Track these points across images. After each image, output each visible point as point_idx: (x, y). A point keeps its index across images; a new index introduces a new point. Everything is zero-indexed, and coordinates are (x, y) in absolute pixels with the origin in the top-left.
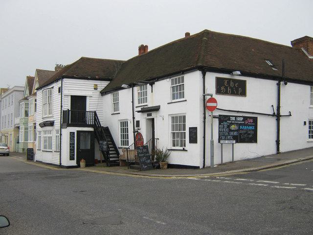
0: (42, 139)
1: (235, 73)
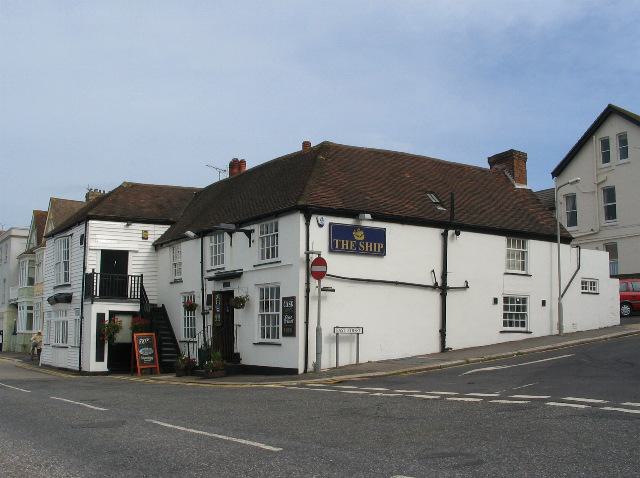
0: (53, 325)
1: (361, 216)
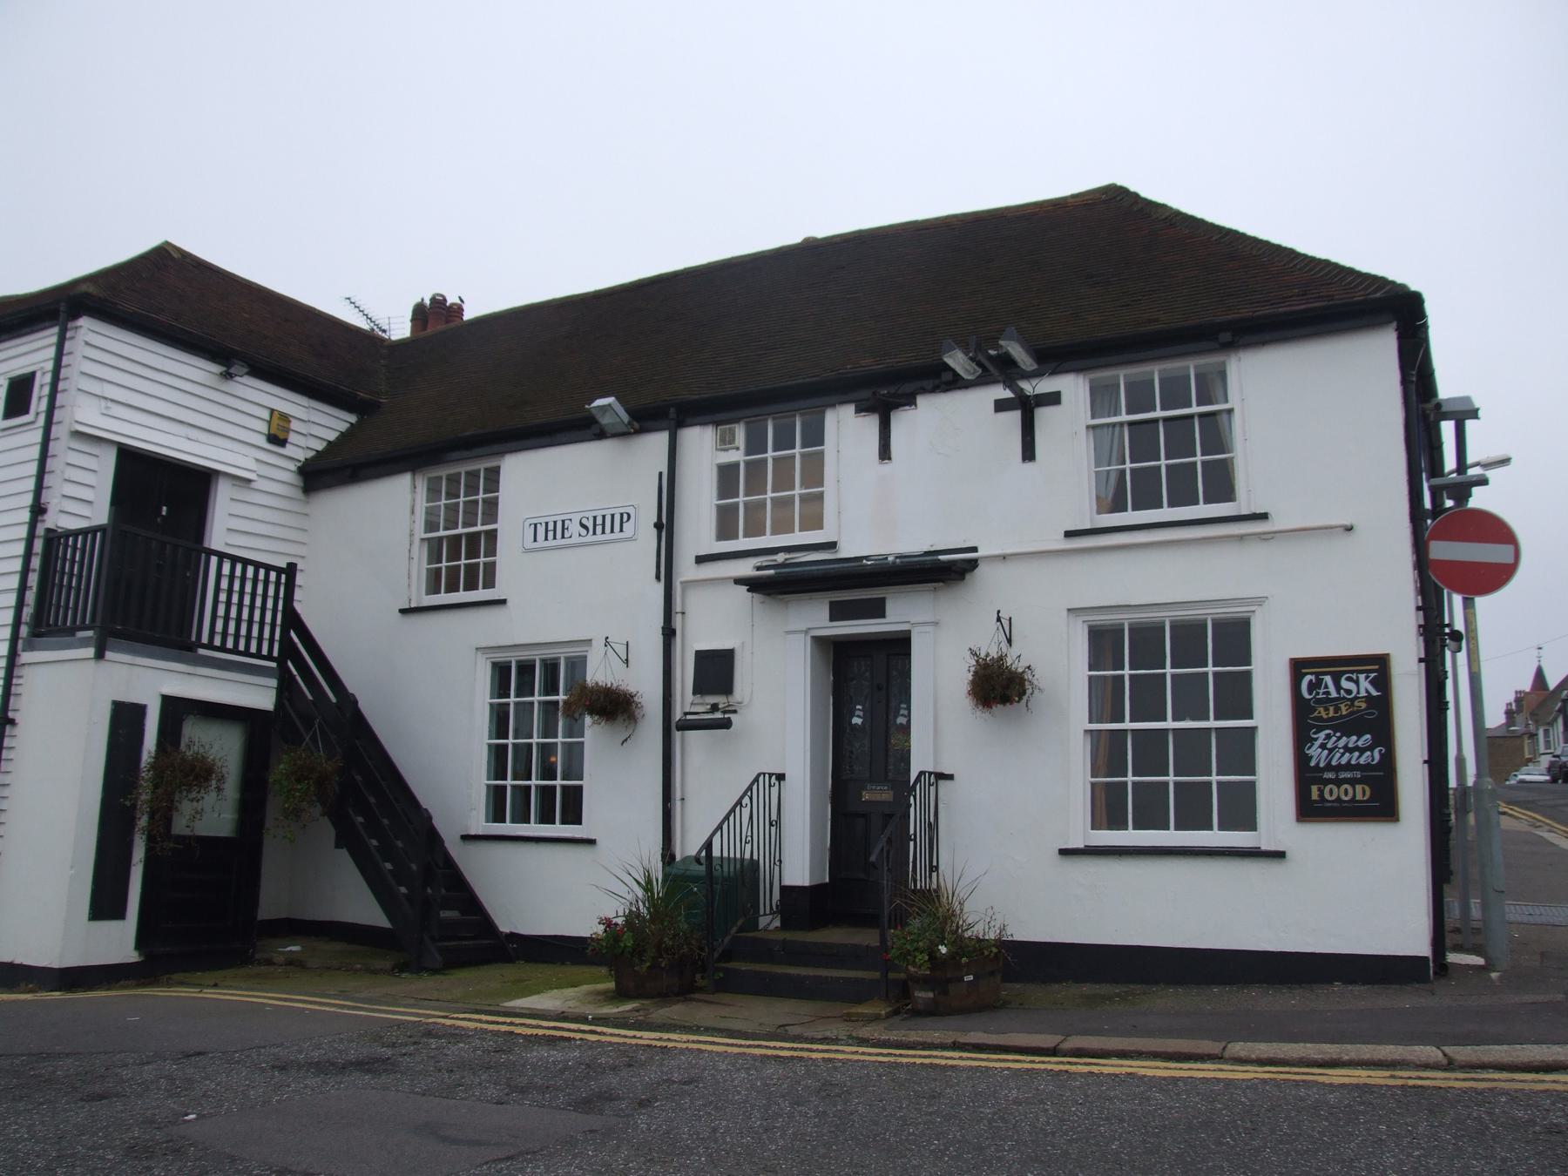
0: (1552, 746)
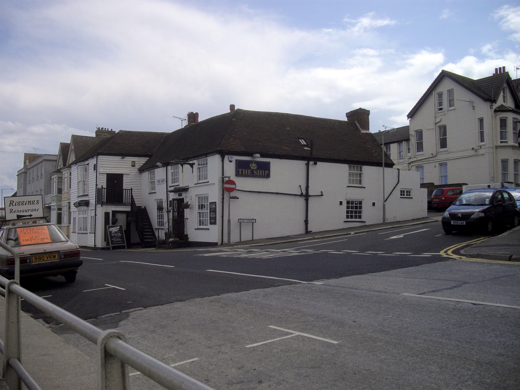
1: (255, 155)
